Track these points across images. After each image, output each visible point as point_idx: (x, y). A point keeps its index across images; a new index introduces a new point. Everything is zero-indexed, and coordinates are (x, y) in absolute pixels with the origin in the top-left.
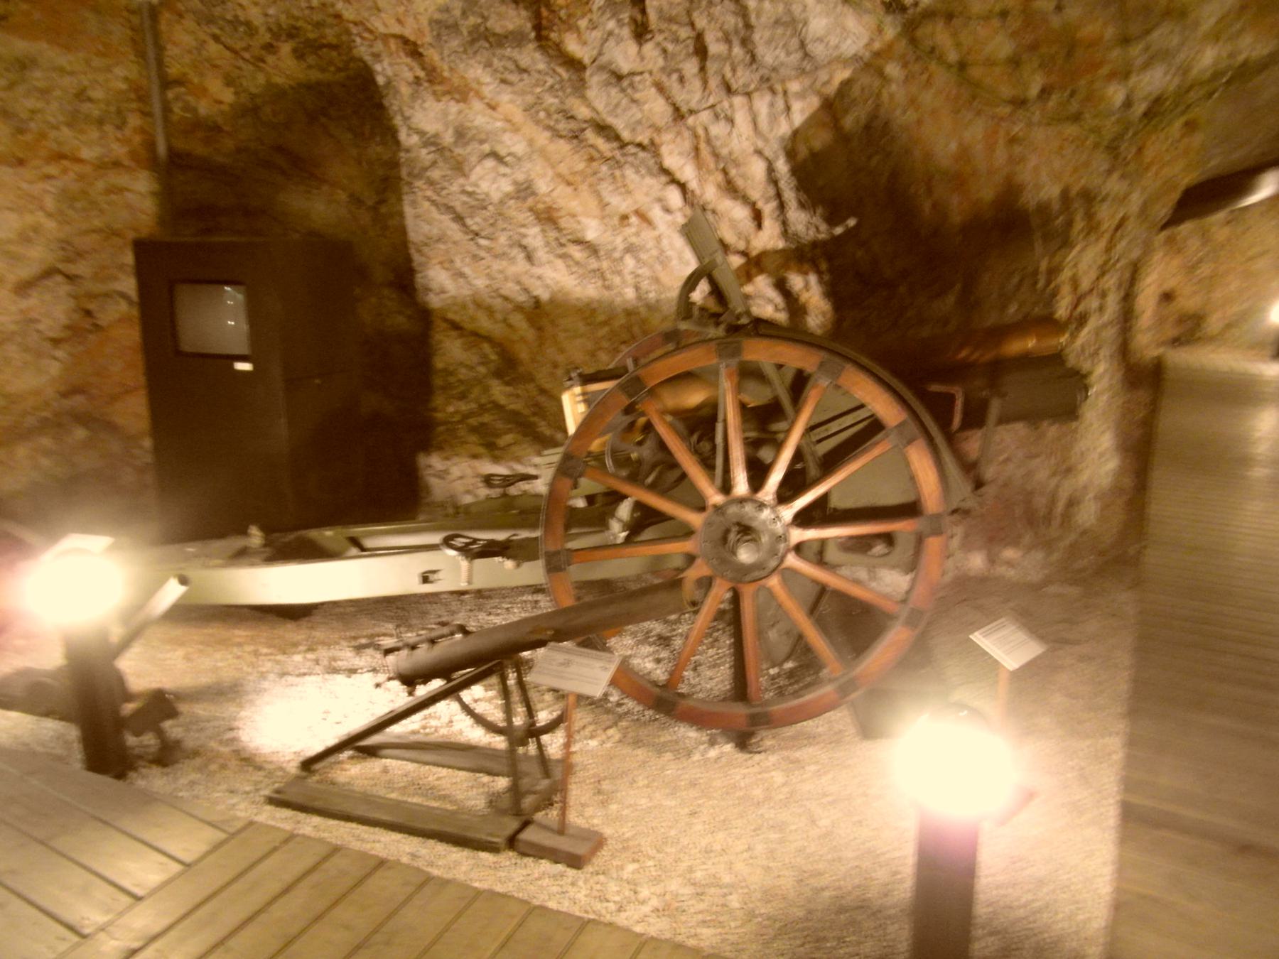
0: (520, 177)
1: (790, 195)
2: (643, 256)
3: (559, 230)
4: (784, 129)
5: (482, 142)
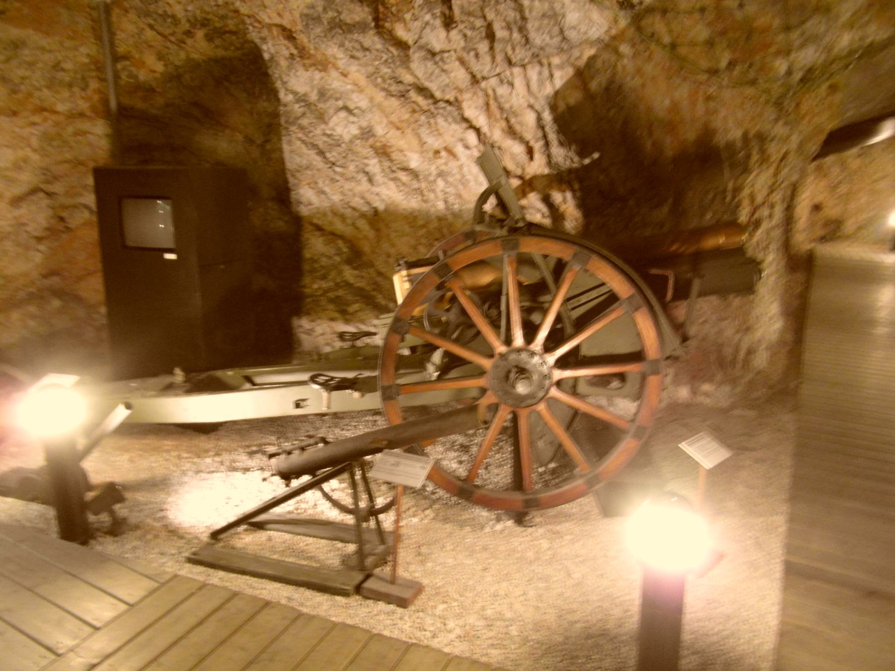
0: (364, 124)
1: (552, 137)
2: (450, 179)
3: (391, 161)
4: (549, 90)
5: (337, 99)
